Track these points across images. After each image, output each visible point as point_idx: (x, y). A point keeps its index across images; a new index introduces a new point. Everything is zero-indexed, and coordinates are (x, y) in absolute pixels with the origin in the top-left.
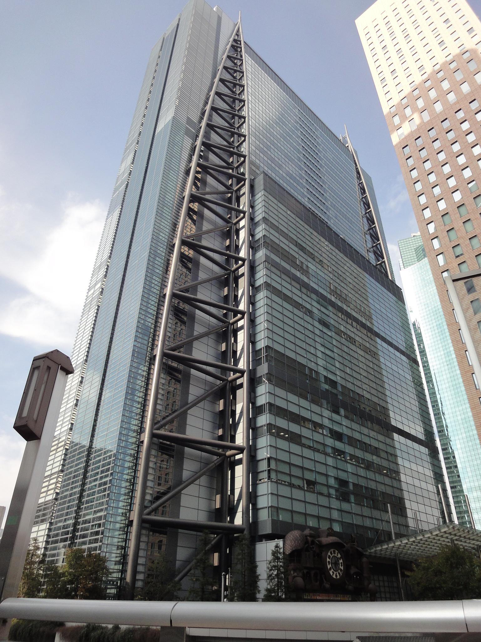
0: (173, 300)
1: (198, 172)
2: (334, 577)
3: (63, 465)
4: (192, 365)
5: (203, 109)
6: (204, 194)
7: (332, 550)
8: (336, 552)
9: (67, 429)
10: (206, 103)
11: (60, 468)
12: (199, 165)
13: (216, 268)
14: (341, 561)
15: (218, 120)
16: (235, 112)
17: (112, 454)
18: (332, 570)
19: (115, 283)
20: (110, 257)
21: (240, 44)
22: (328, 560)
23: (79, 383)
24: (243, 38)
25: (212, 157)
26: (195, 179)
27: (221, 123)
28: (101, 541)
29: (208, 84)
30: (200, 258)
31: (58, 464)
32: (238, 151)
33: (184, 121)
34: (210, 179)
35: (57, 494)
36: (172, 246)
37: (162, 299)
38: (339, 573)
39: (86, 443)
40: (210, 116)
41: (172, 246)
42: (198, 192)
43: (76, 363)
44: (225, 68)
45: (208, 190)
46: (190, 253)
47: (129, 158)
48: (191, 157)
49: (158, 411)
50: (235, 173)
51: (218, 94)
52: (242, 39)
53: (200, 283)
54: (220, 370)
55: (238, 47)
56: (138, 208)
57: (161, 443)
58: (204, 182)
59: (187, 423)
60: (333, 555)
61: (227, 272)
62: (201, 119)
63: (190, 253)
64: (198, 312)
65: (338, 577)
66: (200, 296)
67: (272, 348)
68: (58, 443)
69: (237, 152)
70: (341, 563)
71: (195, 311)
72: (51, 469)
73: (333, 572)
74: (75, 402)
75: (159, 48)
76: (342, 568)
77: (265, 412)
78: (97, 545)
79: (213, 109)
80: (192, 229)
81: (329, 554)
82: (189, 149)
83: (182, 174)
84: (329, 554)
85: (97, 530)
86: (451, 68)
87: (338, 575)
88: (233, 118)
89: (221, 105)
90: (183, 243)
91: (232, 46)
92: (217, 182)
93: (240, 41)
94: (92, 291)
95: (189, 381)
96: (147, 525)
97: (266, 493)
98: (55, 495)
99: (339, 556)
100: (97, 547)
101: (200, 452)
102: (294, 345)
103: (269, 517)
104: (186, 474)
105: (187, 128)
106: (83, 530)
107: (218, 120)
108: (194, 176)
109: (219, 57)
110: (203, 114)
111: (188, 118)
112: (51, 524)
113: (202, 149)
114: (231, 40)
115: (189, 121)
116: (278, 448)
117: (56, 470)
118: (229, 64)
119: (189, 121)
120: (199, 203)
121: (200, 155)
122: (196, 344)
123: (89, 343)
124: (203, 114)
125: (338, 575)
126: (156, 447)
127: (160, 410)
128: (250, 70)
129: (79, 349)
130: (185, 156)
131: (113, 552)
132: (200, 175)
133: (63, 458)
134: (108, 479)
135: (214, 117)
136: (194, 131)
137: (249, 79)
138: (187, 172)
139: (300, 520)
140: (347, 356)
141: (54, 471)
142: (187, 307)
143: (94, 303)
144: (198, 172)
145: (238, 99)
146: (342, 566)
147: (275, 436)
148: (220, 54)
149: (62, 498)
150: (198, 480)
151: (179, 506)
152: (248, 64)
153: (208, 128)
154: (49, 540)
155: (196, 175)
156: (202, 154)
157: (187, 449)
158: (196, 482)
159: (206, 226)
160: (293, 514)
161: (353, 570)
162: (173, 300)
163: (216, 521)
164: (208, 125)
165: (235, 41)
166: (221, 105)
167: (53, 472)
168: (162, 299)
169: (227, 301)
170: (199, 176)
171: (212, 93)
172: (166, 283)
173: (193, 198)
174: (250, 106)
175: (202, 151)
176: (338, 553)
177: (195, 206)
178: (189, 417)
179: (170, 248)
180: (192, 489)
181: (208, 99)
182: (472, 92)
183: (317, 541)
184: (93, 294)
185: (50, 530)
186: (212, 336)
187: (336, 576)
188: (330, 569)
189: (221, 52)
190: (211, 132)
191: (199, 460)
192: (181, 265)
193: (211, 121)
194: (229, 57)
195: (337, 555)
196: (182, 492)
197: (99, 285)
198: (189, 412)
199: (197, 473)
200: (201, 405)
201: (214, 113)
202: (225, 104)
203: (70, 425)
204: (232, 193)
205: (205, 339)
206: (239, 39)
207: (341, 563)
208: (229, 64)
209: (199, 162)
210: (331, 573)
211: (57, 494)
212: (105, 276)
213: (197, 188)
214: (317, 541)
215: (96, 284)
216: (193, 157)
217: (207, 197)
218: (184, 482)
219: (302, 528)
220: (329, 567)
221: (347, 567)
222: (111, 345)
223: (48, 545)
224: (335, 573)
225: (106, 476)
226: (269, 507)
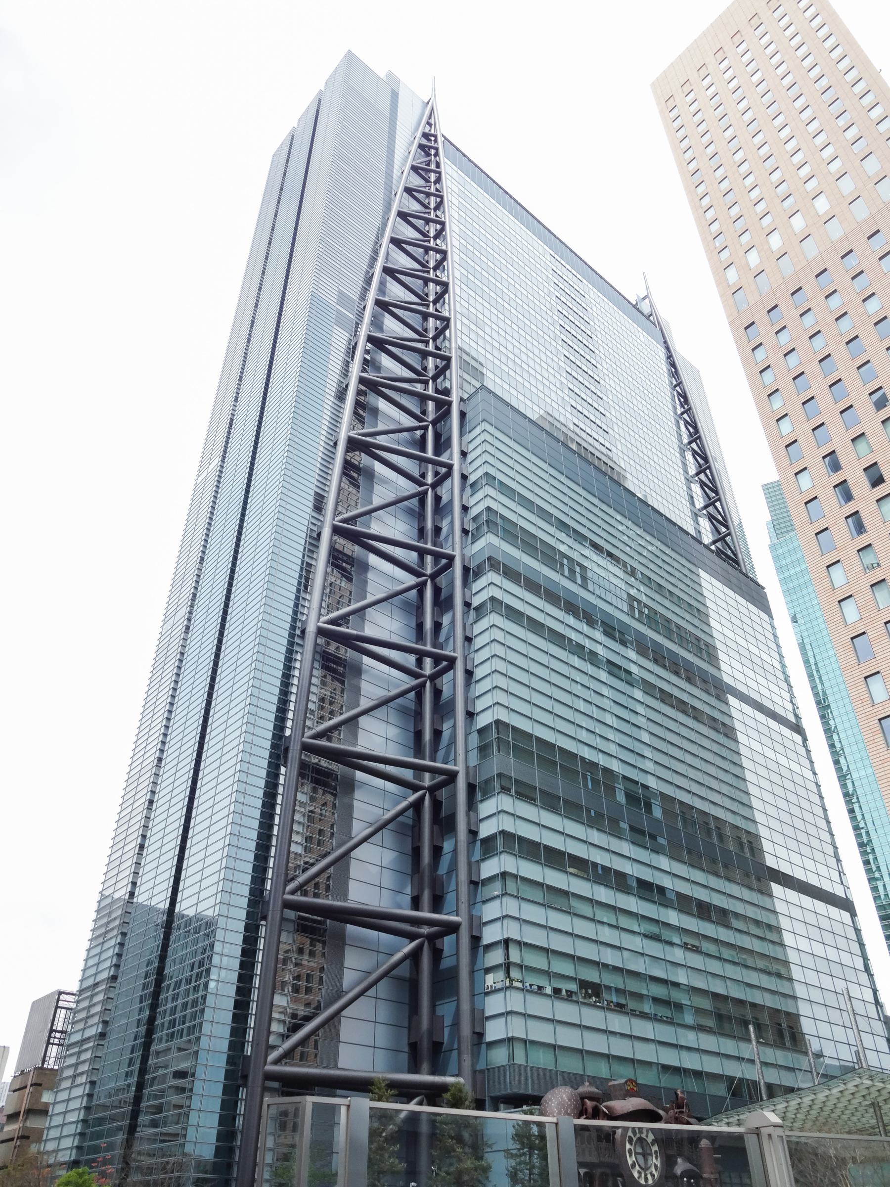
0: (319, 641)
1: (367, 352)
2: (642, 1182)
5: (367, 272)
10: (374, 259)
12: (362, 381)
13: (402, 481)
15: (396, 292)
18: (637, 1168)
21: (436, 141)
22: (628, 1146)
25: (386, 361)
26: (364, 364)
29: (377, 223)
33: (332, 299)
36: (314, 539)
38: (653, 1175)
40: (382, 283)
41: (314, 539)
44: (408, 191)
45: (381, 427)
48: (348, 366)
49: (292, 856)
50: (431, 392)
51: (395, 242)
54: (412, 771)
55: (430, 148)
57: (300, 917)
61: (421, 424)
62: (365, 291)
64: (366, 660)
65: (650, 1182)
66: (369, 631)
67: (507, 725)
68: (108, 923)
69: (435, 277)
70: (656, 1152)
71: (362, 659)
72: (96, 974)
73: (639, 1172)
79: (388, 271)
82: (338, 372)
83: (332, 399)
86: (832, 171)
87: (649, 1176)
88: (427, 252)
89: (402, 261)
92: (400, 366)
93: (435, 136)
94: (171, 622)
96: (276, 1085)
101: (376, 933)
104: (349, 977)
105: (338, 311)
107: (396, 292)
108: (354, 400)
109: (395, 171)
110: (368, 281)
111: (340, 292)
113: (367, 348)
114: (419, 134)
115: (342, 298)
118: (416, 181)
119: (342, 298)
121: (365, 359)
122: (363, 721)
124: (368, 281)
125: (649, 1176)
126: (291, 927)
127: (296, 854)
128: (456, 190)
129: (151, 714)
130: (336, 365)
135: (388, 285)
136: (351, 316)
137: (454, 220)
138: (341, 396)
139: (570, 1064)
140: (708, 949)
142: (347, 653)
146: (657, 1158)
148: (399, 164)
151: (337, 1041)
152: (448, 168)
153: (377, 308)
156: (368, 357)
157: (350, 928)
159: (380, 495)
161: (681, 1166)
163: (415, 757)
164: (378, 303)
165: (426, 136)
166: (402, 261)
167: (97, 980)
169: (416, 1066)
171: (386, 240)
173: (353, 444)
174: (459, 327)
175: (367, 352)
178: (353, 864)
179: (311, 541)
180: (362, 1008)
181: (376, 252)
182: (872, 216)
183: (606, 1107)
186: (386, 836)
187: (646, 1179)
188: (633, 1165)
189: (400, 160)
190: (383, 316)
192: (348, 482)
193: (381, 329)
194: (414, 169)
196: (343, 1013)
198: (354, 854)
199: (370, 973)
200: (376, 838)
201: (388, 278)
202: (409, 259)
204: (426, 428)
205: (381, 712)
207: (656, 1152)
208: (416, 181)
209: (365, 375)
210: (636, 1175)
214: (606, 1107)
216: (351, 365)
217: (381, 440)
218: (347, 993)
219: (573, 1080)
220: (630, 1162)
223: (82, 1155)
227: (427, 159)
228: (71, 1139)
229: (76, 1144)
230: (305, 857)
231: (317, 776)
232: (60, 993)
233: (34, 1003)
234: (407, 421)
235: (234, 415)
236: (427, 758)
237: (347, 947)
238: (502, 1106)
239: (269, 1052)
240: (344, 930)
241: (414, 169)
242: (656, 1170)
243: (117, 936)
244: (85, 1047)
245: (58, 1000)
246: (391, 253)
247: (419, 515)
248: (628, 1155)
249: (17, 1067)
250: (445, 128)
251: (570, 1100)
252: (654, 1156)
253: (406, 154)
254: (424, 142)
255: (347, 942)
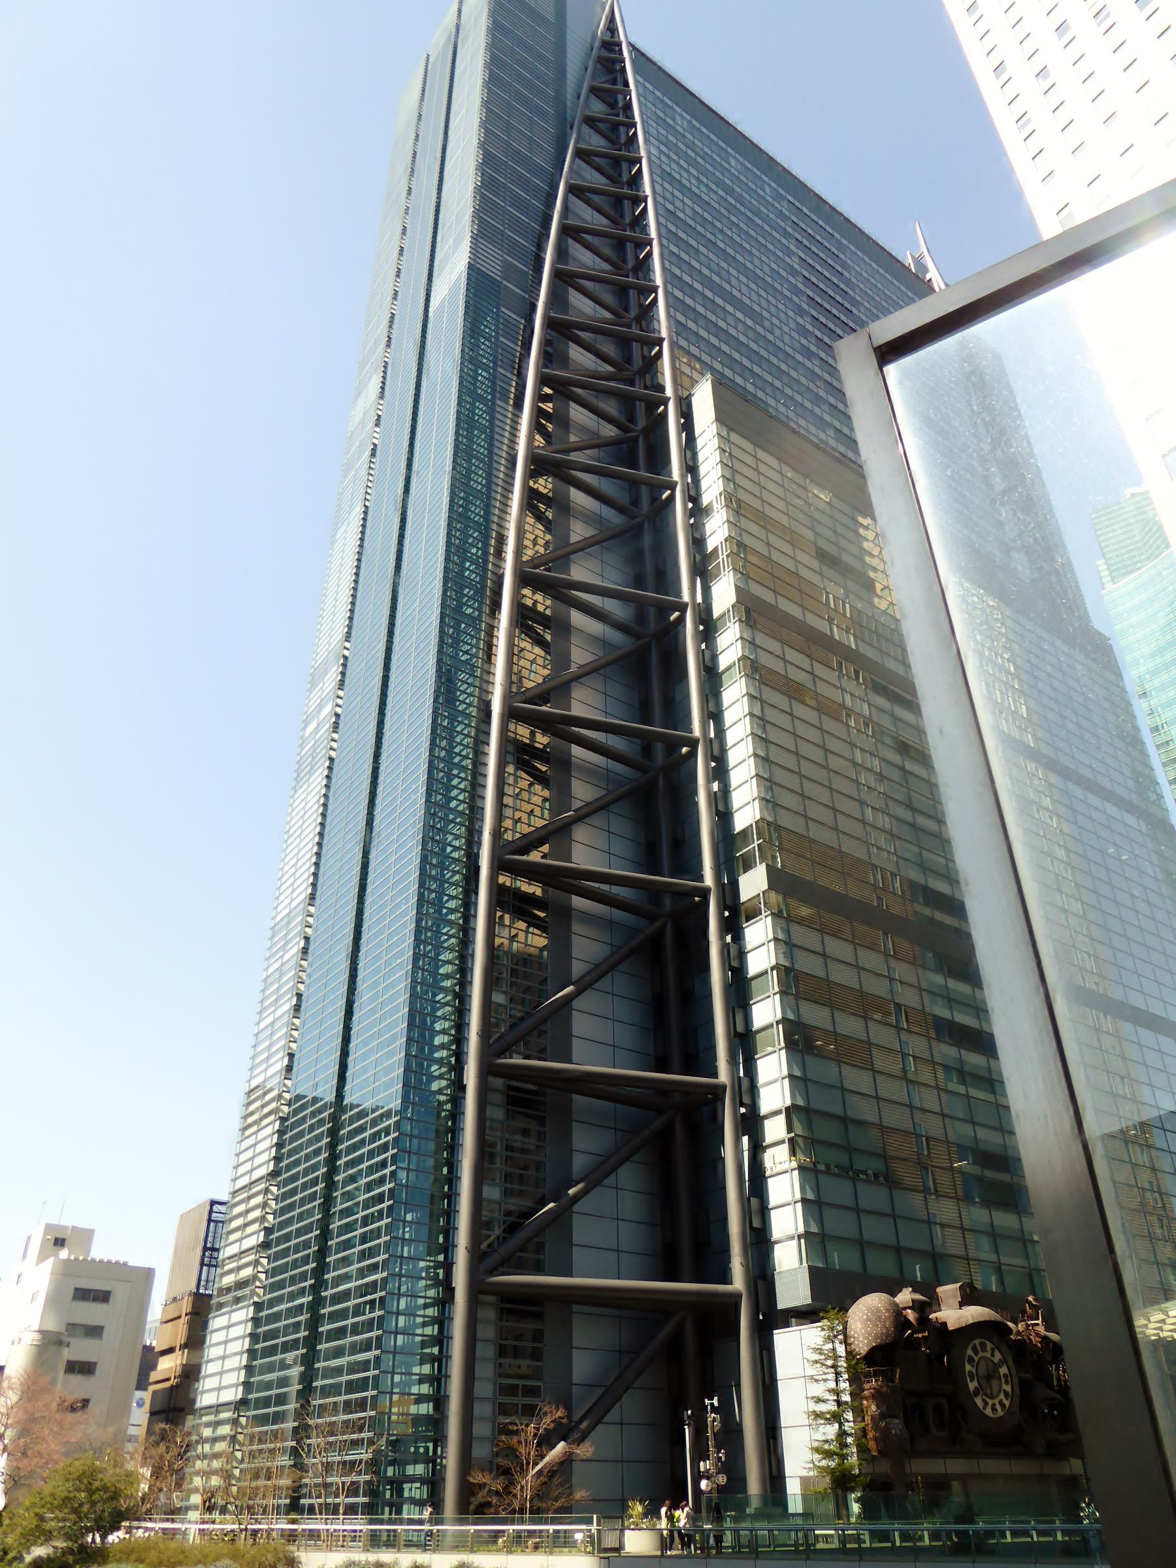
2: (988, 1411)
3: (278, 1159)
4: (574, 477)
6: (567, 451)
7: (977, 1342)
8: (989, 1345)
9: (281, 1070)
11: (261, 1239)
14: (1004, 1370)
16: (630, 327)
17: (390, 1125)
19: (368, 688)
20: (348, 637)
22: (968, 1367)
23: (307, 901)
24: (626, 35)
25: (576, 354)
26: (538, 417)
27: (590, 263)
28: (373, 1408)
30: (569, 616)
31: (265, 1157)
32: (642, 330)
34: (577, 413)
35: (268, 1231)
37: (483, 727)
39: (331, 1097)
42: (550, 448)
43: (290, 904)
44: (590, 121)
45: (573, 438)
46: (543, 603)
47: (353, 514)
52: (622, 38)
53: (577, 678)
56: (401, 537)
57: (510, 1088)
58: (562, 421)
59: (574, 1033)
60: (981, 1354)
63: (543, 603)
66: (578, 710)
73: (984, 1401)
74: (294, 1001)
75: (304, 890)
76: (1008, 1388)
77: (730, 621)
78: (370, 1355)
80: (537, 671)
81: (970, 1352)
84: (970, 1352)
85: (384, 1140)
87: (998, 1407)
89: (587, 216)
90: (524, 579)
91: (600, 60)
95: (570, 952)
97: (789, 1198)
98: (262, 1233)
99: (997, 1357)
100: (368, 1361)
102: (781, 489)
103: (801, 1263)
104: (579, 1162)
106: (334, 1317)
108: (535, 409)
112: (258, 1306)
116: (770, 742)
117: (263, 1171)
120: (555, 476)
123: (315, 863)
125: (998, 1407)
131: (418, 1313)
132: (550, 405)
133: (275, 1140)
134: (386, 1188)
135: (571, 250)
141: (257, 1175)
143: (323, 753)
144: (545, 398)
145: (627, 197)
146: (1007, 1382)
147: (801, 1051)
149: (279, 1241)
150: (613, 1176)
154: (257, 1346)
155: (540, 405)
158: (607, 1182)
159: (579, 531)
160: (862, 1216)
162: (512, 726)
166: (587, 216)
168: (483, 727)
170: (548, 407)
172: (491, 675)
176: (993, 1350)
177: (544, 485)
184: (316, 730)
185: (256, 1321)
187: (994, 1409)
191: (606, 776)
194: (594, 91)
195: (993, 1355)
196: (575, 1208)
197: (328, 708)
201: (570, 241)
203: (295, 999)
206: (616, 39)
208: (598, 108)
211: (283, 1120)
212: (341, 684)
213: (546, 436)
215: (320, 707)
217: (574, 457)
221: (1025, 1388)
222: (389, 663)
224: (990, 1402)
225: (382, 1181)
226: (799, 1237)
227: (611, 76)
228: (243, 1326)
229: (248, 1331)
230: (511, 1010)
231: (519, 904)
232: (213, 1203)
233: (182, 1216)
234: (609, 431)
235: (264, 1513)
236: (666, 871)
237: (574, 1124)
238: (793, 1320)
239: (638, 741)
240: (571, 1099)
241: (594, 91)
242: (1007, 1399)
243: (283, 1057)
244: (254, 1191)
245: (211, 1212)
246: (571, 205)
247: (636, 557)
248: (968, 1379)
249: (168, 1292)
250: (631, 33)
251: (887, 1311)
252: (1003, 1380)
253: (589, 52)
254: (605, 54)
255: (575, 1117)
